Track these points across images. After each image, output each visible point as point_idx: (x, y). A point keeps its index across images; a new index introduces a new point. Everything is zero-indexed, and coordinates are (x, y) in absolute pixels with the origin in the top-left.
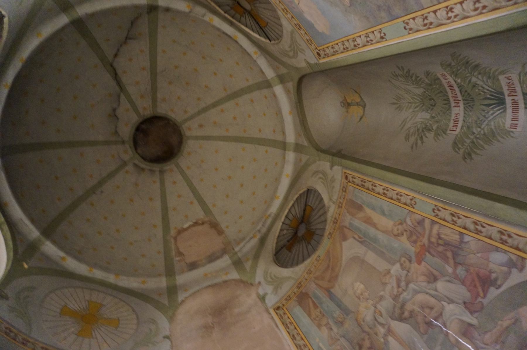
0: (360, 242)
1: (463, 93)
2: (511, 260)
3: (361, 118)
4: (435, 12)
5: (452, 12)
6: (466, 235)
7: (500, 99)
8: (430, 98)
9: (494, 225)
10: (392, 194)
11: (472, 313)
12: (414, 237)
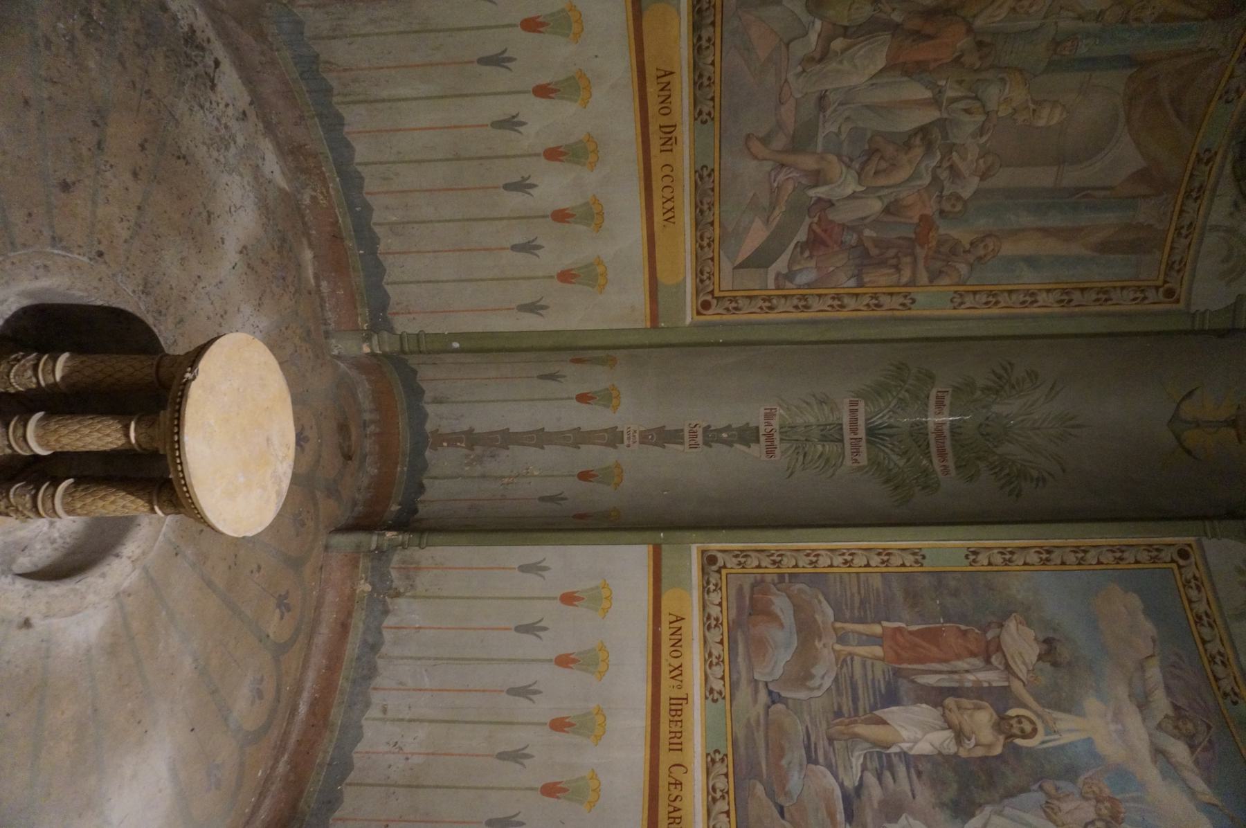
0: (1083, 189)
1: (926, 443)
2: (791, 281)
3: (1190, 394)
4: (868, 565)
5: (845, 560)
7: (874, 435)
8: (988, 437)
9: (818, 313)
10: (1011, 299)
11: (819, 200)
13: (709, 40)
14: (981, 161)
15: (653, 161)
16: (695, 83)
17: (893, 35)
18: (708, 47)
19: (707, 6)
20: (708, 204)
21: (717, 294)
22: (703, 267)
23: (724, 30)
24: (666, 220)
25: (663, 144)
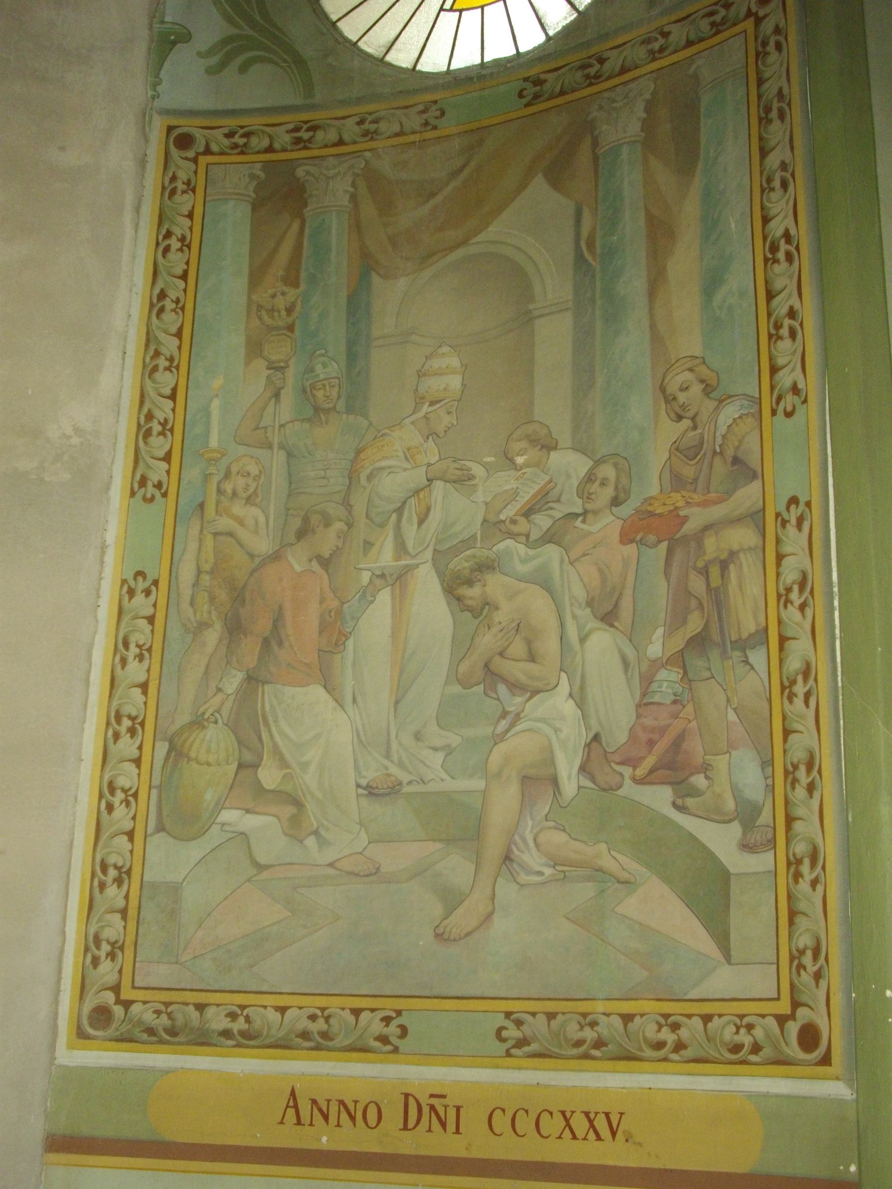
6: (759, 432)
12: (688, 471)
13: (233, 1016)
14: (520, 460)
15: (477, 1153)
16: (318, 1048)
17: (264, 683)
18: (248, 1019)
19: (164, 1017)
20: (582, 1028)
21: (784, 1007)
22: (645, 1040)
23: (216, 987)
24: (614, 1134)
25: (443, 1125)
